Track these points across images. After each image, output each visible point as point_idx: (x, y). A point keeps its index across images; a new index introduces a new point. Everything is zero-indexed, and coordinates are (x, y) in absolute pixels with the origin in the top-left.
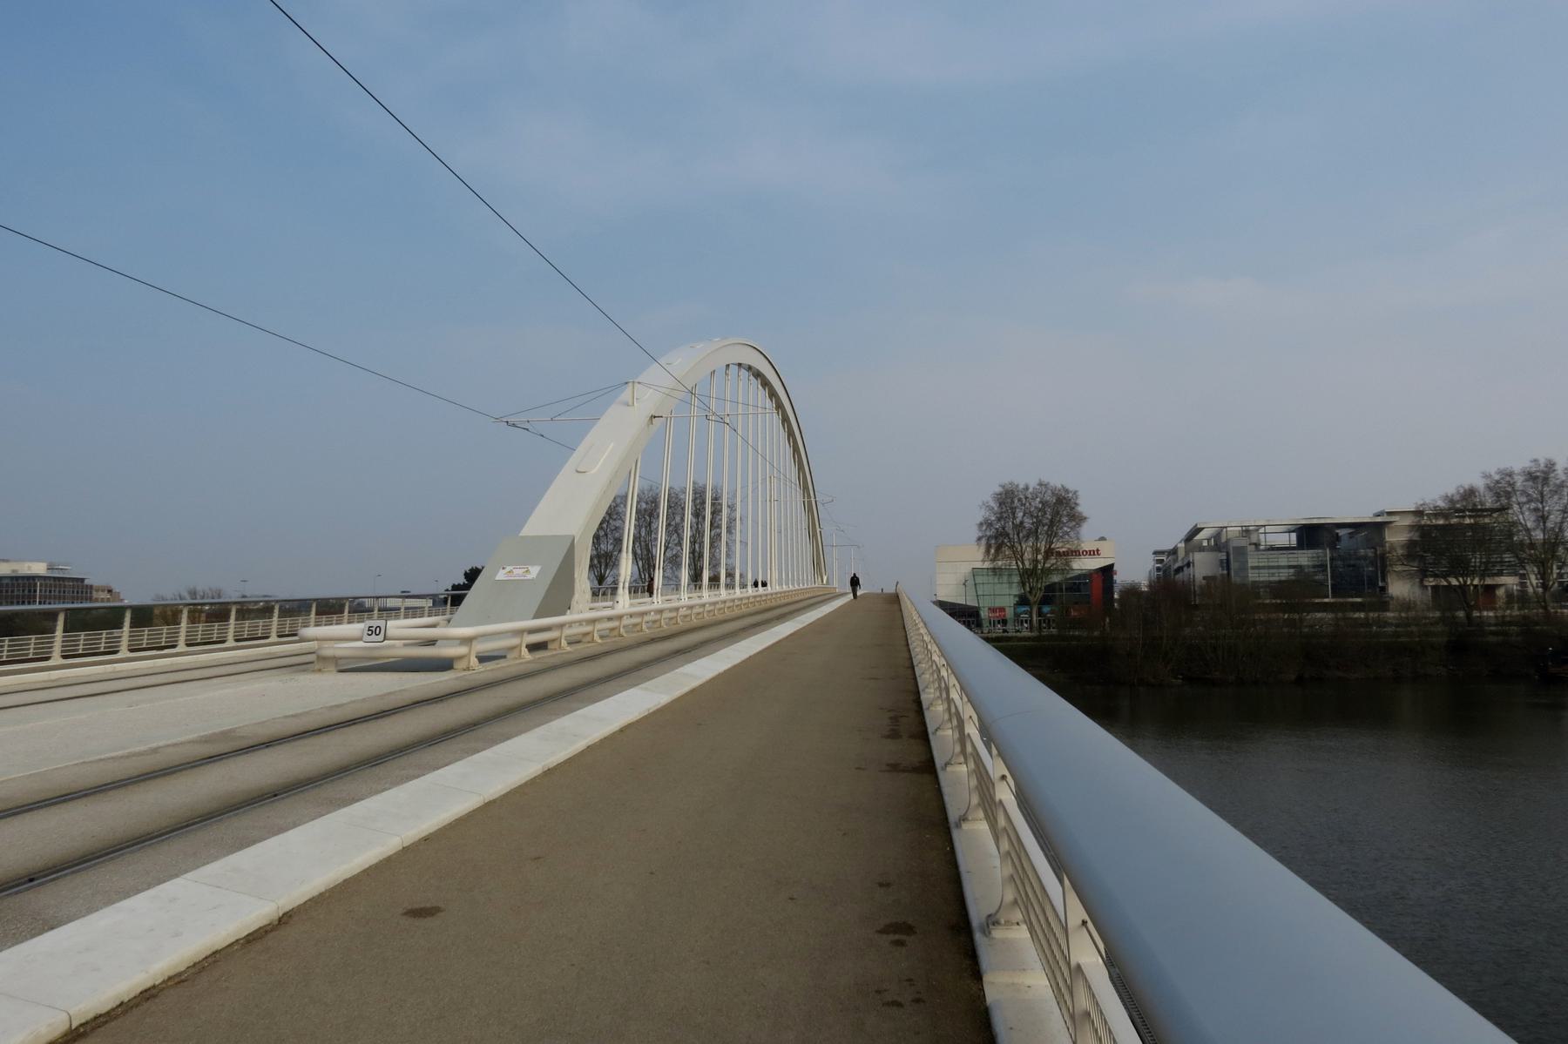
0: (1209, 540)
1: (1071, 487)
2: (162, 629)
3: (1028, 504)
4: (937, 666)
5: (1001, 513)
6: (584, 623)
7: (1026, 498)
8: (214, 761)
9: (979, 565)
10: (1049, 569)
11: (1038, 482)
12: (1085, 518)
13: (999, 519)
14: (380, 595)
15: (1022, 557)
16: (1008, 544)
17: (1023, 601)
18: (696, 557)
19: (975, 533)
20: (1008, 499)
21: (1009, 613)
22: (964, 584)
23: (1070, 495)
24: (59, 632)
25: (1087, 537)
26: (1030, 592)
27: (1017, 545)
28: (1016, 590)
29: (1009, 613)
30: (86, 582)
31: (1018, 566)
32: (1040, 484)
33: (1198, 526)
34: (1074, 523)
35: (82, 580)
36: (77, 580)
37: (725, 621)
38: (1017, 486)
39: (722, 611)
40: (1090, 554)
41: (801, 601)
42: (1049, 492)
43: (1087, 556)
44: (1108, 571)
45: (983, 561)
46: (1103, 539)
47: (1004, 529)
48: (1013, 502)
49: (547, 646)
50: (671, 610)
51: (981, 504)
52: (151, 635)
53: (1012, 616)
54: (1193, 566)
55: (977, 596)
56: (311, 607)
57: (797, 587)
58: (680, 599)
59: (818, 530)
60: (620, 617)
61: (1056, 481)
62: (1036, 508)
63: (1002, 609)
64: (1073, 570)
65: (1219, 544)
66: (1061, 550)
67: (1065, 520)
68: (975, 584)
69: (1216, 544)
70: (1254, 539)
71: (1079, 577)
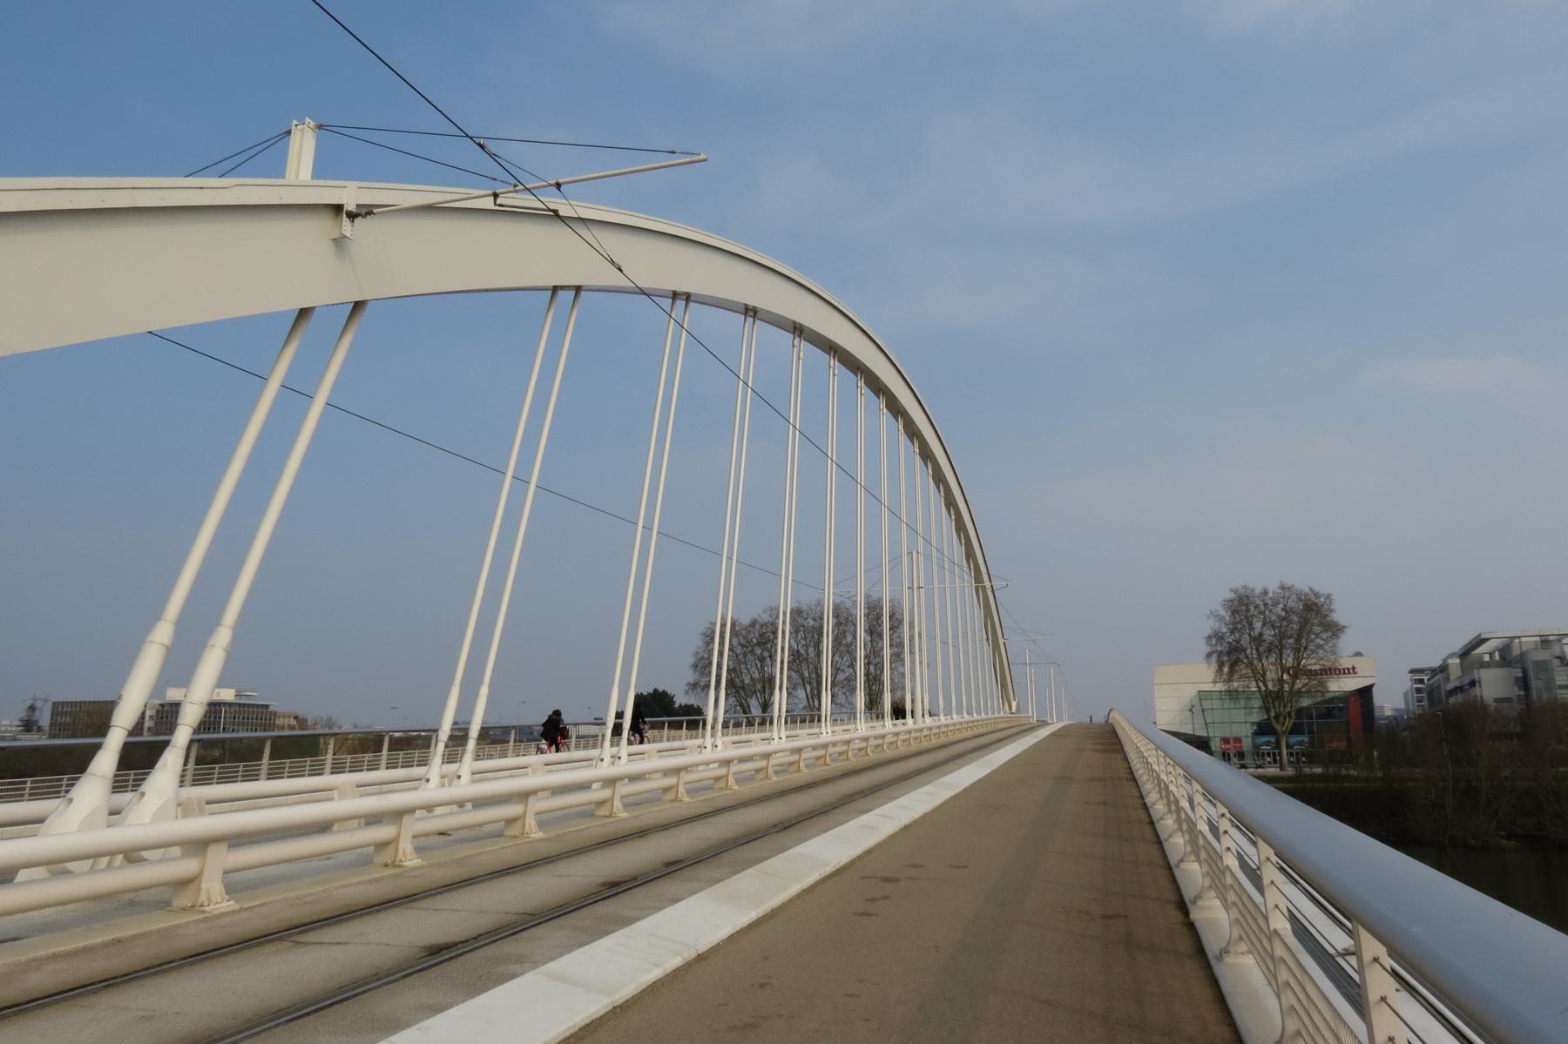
0: (1491, 654)
1: (1322, 589)
2: (458, 750)
3: (1267, 612)
4: (1165, 784)
5: (1234, 623)
6: (469, 805)
7: (1266, 605)
8: (627, 840)
9: (1209, 687)
10: (1299, 691)
11: (1278, 584)
12: (1344, 627)
13: (1232, 632)
14: (578, 722)
15: (1264, 675)
16: (1245, 661)
17: (1263, 729)
18: (874, 682)
19: (1204, 648)
20: (1242, 607)
21: (1247, 744)
22: (1191, 710)
23: (1322, 600)
24: (511, 743)
25: (1346, 646)
26: (1276, 718)
27: (1255, 662)
28: (1256, 717)
29: (1247, 744)
30: (271, 709)
31: (1259, 687)
32: (1283, 588)
33: (1483, 637)
34: (1330, 634)
35: (267, 707)
36: (262, 706)
37: (826, 781)
38: (1253, 590)
39: (907, 743)
40: (1344, 673)
41: (1004, 729)
42: (1294, 596)
43: (1333, 676)
44: (1365, 693)
45: (1215, 682)
46: (1358, 654)
47: (1238, 642)
48: (1248, 610)
49: (506, 823)
50: (876, 738)
51: (1209, 613)
52: (292, 767)
53: (1250, 748)
54: (1480, 686)
55: (1206, 724)
56: (683, 724)
57: (990, 715)
58: (703, 747)
59: (1001, 641)
60: (825, 746)
61: (1304, 581)
62: (1278, 616)
63: (1238, 740)
64: (1329, 692)
65: (1506, 656)
66: (1314, 668)
67: (1317, 629)
68: (1203, 710)
69: (1503, 658)
70: (1556, 650)
71: (1331, 700)
